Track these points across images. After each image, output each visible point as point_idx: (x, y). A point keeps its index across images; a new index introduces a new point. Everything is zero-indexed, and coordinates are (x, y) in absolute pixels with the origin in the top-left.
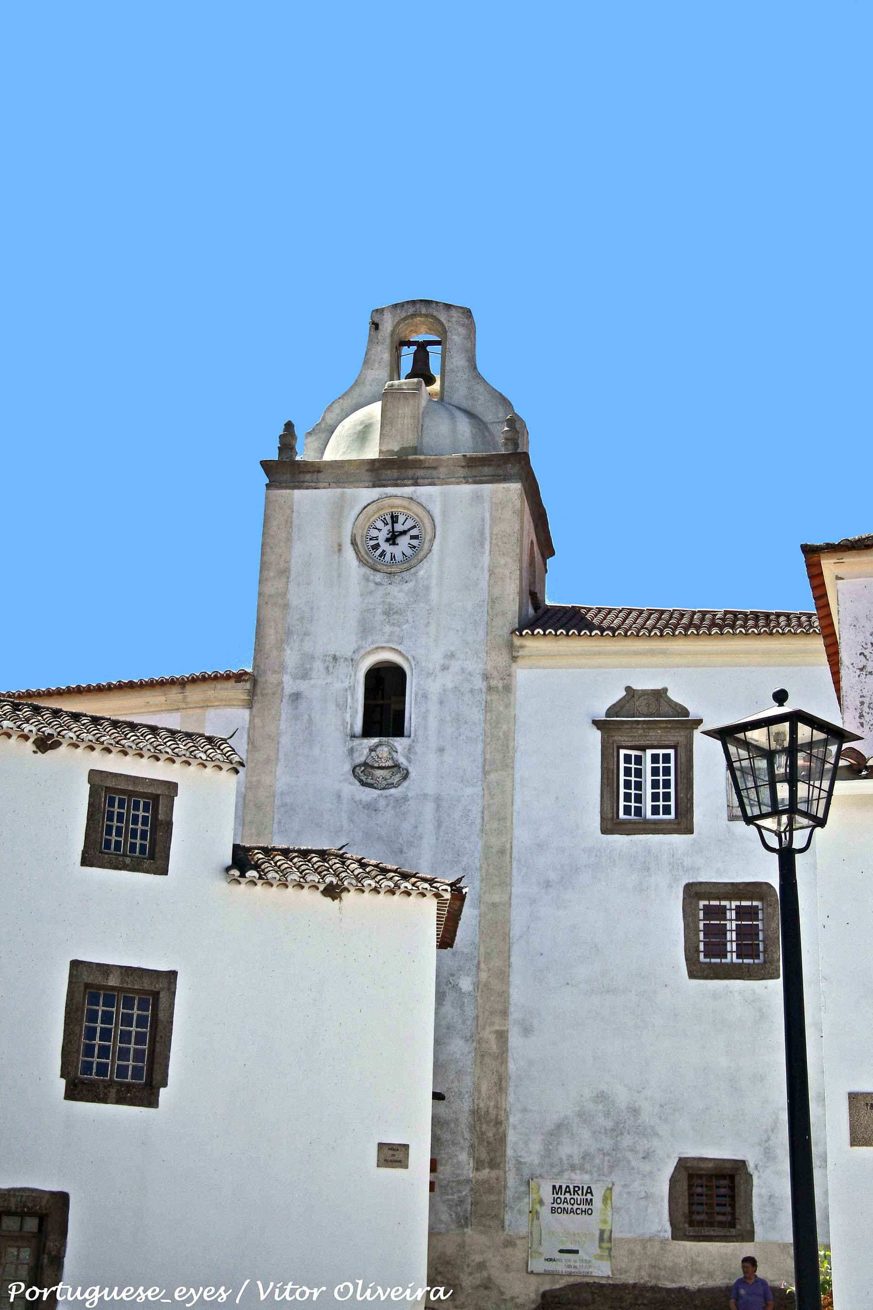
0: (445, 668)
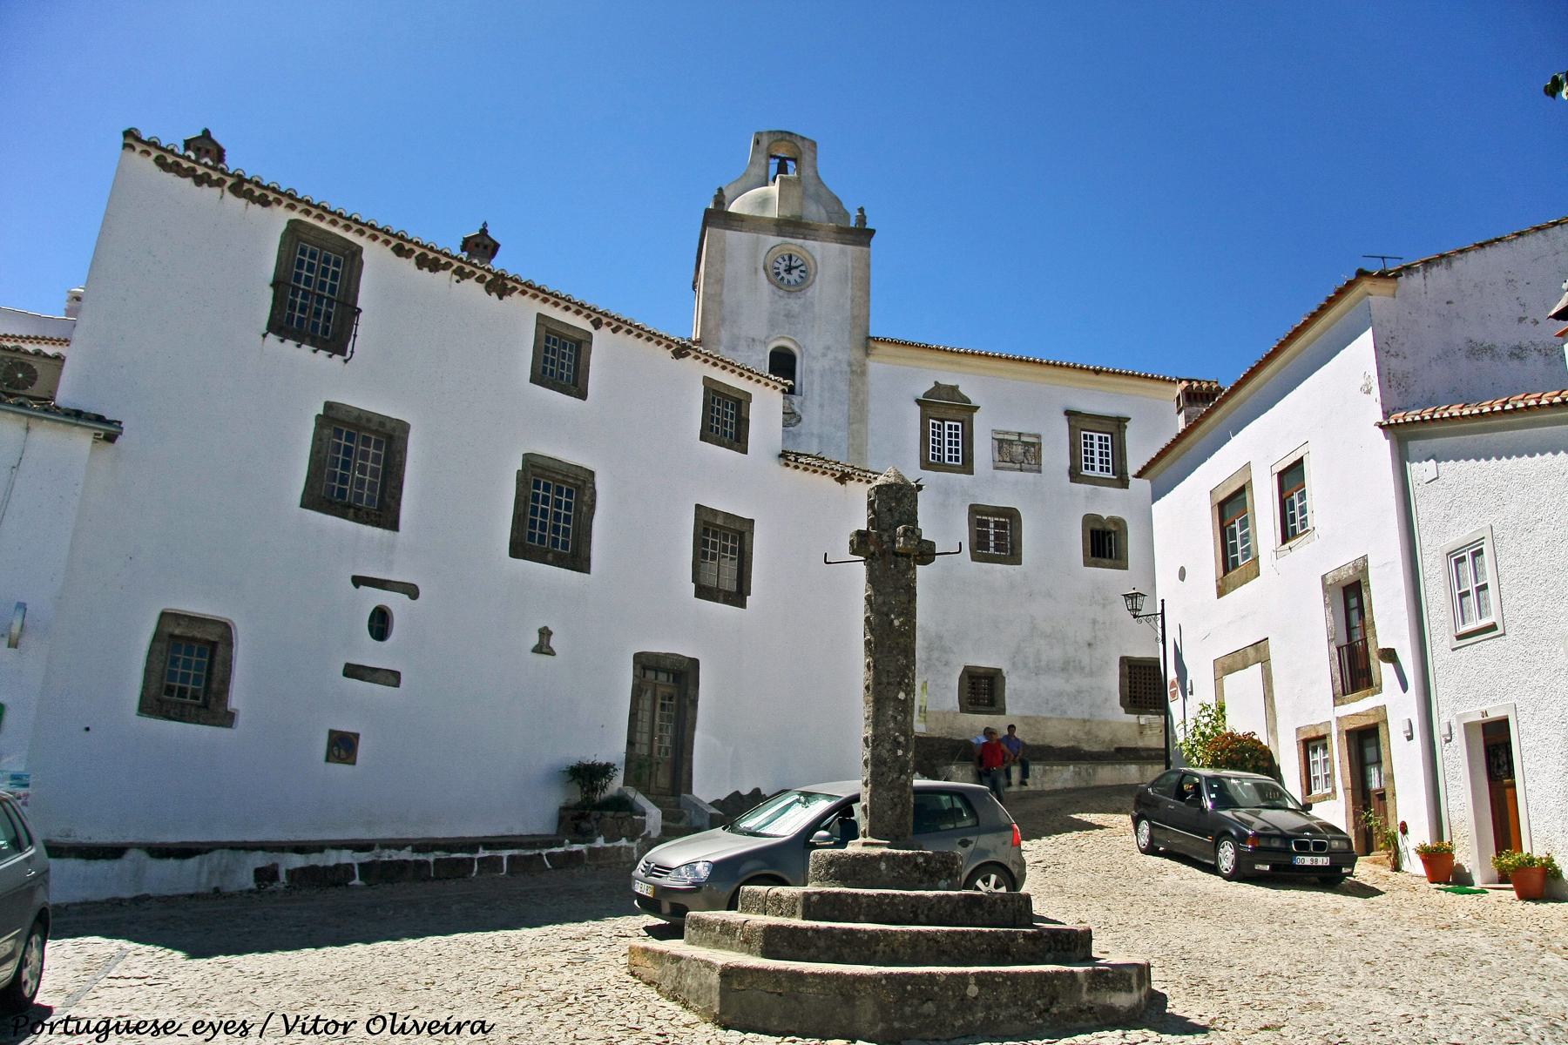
0: (824, 355)
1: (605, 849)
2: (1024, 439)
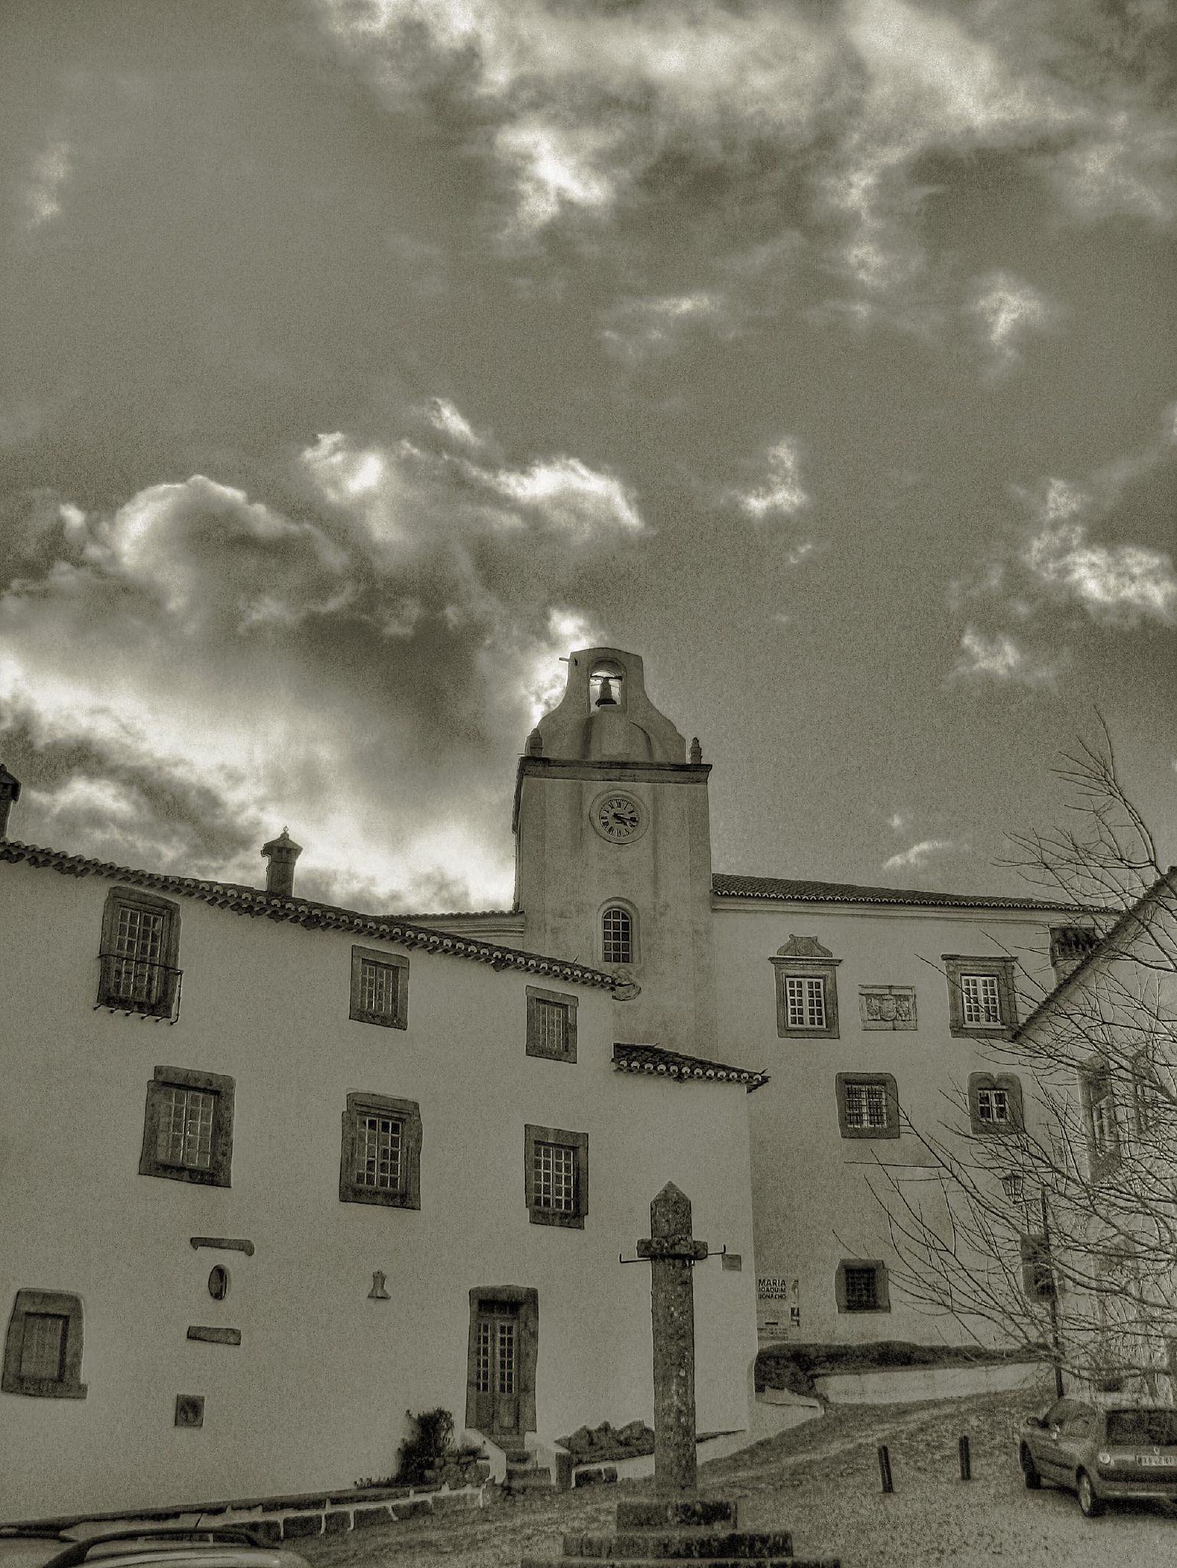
1: (449, 1498)
2: (895, 992)
